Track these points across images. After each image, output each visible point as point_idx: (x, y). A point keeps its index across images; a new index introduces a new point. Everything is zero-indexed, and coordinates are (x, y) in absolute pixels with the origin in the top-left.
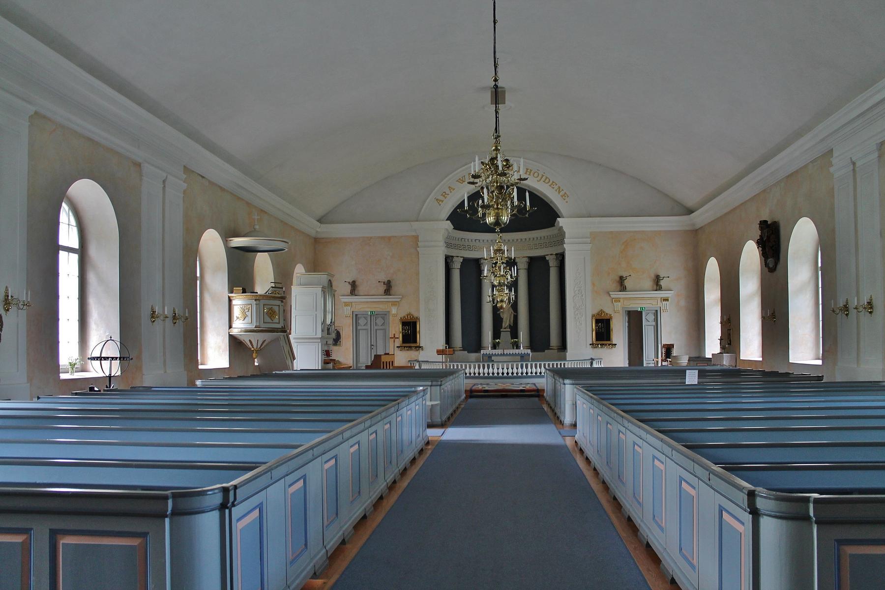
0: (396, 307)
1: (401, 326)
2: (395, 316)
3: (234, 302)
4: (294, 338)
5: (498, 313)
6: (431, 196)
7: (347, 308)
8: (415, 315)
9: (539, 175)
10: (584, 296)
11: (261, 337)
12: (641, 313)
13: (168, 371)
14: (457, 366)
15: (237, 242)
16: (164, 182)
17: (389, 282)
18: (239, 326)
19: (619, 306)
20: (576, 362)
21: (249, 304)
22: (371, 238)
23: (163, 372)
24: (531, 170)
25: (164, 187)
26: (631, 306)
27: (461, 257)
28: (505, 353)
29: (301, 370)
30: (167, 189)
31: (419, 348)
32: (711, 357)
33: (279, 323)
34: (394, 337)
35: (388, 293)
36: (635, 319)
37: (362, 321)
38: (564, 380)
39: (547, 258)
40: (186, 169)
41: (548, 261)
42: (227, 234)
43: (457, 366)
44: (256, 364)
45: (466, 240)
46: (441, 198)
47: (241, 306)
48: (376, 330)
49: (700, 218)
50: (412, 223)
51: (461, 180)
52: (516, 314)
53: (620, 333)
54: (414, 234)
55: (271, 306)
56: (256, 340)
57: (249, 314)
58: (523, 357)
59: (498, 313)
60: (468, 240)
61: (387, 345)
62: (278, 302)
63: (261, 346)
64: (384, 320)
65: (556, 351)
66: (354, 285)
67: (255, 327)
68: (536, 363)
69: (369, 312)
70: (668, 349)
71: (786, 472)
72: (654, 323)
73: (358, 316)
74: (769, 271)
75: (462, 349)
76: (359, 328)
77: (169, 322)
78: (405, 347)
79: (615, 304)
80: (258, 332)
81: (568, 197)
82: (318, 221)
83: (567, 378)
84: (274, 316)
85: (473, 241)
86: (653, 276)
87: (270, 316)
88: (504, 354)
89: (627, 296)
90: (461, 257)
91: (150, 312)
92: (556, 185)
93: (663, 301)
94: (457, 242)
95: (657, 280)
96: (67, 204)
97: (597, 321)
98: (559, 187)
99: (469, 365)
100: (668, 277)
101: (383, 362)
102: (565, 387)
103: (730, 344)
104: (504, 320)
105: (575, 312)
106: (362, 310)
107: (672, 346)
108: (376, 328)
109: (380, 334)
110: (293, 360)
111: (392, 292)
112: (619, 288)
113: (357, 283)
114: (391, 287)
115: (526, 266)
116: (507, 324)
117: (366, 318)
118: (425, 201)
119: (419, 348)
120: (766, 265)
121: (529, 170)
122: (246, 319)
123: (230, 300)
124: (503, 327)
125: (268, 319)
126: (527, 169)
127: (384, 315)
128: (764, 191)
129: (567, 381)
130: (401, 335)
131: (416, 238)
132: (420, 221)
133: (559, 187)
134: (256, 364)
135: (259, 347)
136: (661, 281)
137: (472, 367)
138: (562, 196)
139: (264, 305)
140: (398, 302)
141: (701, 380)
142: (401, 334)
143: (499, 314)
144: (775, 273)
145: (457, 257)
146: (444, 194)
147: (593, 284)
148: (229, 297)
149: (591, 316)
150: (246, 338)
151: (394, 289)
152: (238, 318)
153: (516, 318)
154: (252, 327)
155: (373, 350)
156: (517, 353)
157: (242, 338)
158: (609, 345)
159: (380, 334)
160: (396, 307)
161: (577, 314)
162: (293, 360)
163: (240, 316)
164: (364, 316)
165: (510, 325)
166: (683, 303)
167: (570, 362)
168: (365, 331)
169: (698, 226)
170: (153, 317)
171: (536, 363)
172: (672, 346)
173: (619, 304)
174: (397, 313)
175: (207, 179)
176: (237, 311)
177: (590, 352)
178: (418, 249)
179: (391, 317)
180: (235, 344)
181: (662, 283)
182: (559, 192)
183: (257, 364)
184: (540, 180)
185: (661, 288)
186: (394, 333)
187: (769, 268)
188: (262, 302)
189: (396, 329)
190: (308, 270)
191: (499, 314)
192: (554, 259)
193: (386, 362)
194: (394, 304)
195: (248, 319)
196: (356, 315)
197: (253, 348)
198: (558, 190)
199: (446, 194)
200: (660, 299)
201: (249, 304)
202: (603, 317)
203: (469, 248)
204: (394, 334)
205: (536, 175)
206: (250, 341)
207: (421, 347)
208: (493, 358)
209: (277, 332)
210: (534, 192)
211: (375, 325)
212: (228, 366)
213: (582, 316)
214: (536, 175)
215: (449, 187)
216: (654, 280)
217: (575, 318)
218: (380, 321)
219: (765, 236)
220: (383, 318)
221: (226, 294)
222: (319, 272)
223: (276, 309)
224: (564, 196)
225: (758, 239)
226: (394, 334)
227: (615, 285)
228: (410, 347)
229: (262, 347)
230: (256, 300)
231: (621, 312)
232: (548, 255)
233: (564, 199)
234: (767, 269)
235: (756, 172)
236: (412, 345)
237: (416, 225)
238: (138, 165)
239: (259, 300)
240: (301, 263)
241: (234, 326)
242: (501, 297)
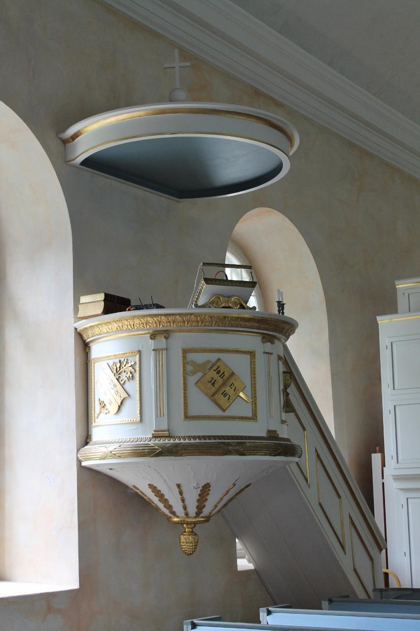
3: (96, 351)
4: (397, 478)
33: (254, 418)
44: (244, 564)
55: (213, 357)
57: (133, 387)
62: (251, 341)
67: (155, 437)
71: (50, 162)
84: (230, 391)
96: (234, 255)
110: (373, 550)
122: (125, 409)
123: (84, 346)
125: (201, 404)
134: (244, 564)
135: (192, 510)
141: (378, 451)
148: (79, 335)
162: (373, 550)
183: (251, 566)
188: (180, 340)
195: (132, 409)
206: (153, 488)
209: (242, 454)
223: (239, 365)
239: (166, 334)
241: (97, 434)
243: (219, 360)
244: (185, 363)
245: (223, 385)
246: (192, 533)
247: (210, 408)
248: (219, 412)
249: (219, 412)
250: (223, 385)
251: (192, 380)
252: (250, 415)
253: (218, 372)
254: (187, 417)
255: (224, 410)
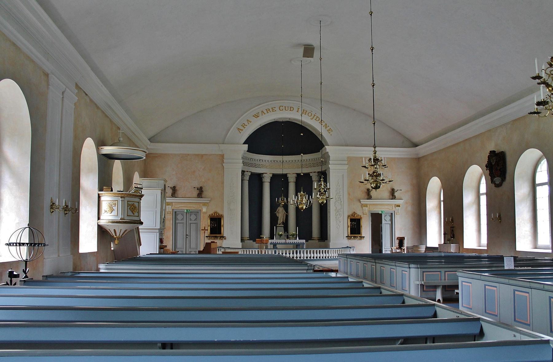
0: (206, 207)
1: (209, 221)
2: (206, 213)
3: (102, 198)
5: (275, 213)
6: (233, 126)
7: (169, 207)
8: (220, 213)
9: (312, 114)
10: (342, 202)
11: (124, 227)
12: (381, 215)
13: (60, 256)
14: (255, 252)
15: (107, 150)
16: (63, 93)
17: (201, 188)
18: (107, 217)
19: (366, 209)
20: (337, 249)
21: (116, 201)
22: (188, 155)
23: (57, 256)
24: (306, 111)
25: (63, 100)
26: (375, 210)
27: (250, 172)
28: (287, 242)
29: (151, 254)
30: (65, 99)
31: (223, 237)
32: (438, 246)
34: (205, 229)
35: (200, 197)
36: (377, 219)
37: (179, 217)
38: (409, 265)
39: (311, 175)
40: (77, 86)
41: (311, 176)
42: (100, 143)
43: (255, 252)
44: (112, 249)
45: (254, 160)
46: (242, 128)
47: (109, 202)
48: (190, 224)
49: (422, 150)
50: (220, 145)
51: (256, 116)
52: (287, 214)
53: (366, 229)
54: (220, 153)
55: (133, 203)
56: (120, 229)
57: (115, 208)
58: (297, 246)
59: (275, 213)
60: (255, 160)
61: (198, 235)
63: (122, 235)
64: (196, 216)
65: (317, 241)
66: (174, 189)
67: (120, 219)
68: (317, 250)
69: (185, 211)
70: (401, 241)
72: (390, 222)
73: (177, 213)
74: (495, 186)
75: (249, 239)
76: (177, 222)
77: (62, 213)
78: (212, 237)
79: (397, 208)
80: (123, 223)
81: (332, 131)
82: (149, 140)
83: (413, 263)
85: (259, 160)
86: (390, 189)
87: (132, 210)
88: (286, 243)
89: (372, 203)
90: (250, 172)
91: (49, 204)
92: (324, 122)
93: (397, 207)
94: (254, 161)
95: (393, 192)
97: (352, 220)
98: (326, 124)
99: (282, 250)
100: (401, 190)
101: (212, 248)
102: (410, 270)
103: (453, 237)
104: (279, 219)
105: (336, 213)
106: (180, 208)
107: (403, 238)
108: (190, 222)
109: (193, 227)
110: (139, 246)
111: (203, 196)
112: (366, 197)
113: (177, 188)
114: (203, 192)
115: (295, 180)
116: (282, 221)
117: (182, 215)
118: (229, 130)
119: (223, 237)
120: (492, 181)
121: (305, 111)
122: (112, 213)
123: (99, 197)
124: (278, 224)
126: (266, 110)
127: (197, 213)
128: (490, 131)
129: (412, 266)
130: (209, 228)
131: (222, 156)
132: (225, 144)
133: (326, 124)
135: (121, 235)
136: (395, 193)
137: (291, 253)
138: (328, 131)
139: (127, 201)
140: (207, 203)
142: (209, 227)
143: (276, 213)
144: (500, 188)
145: (247, 171)
146: (244, 125)
147: (349, 194)
148: (99, 194)
149: (347, 217)
150: (111, 228)
151: (205, 194)
152: (106, 211)
153: (287, 217)
154: (118, 219)
155: (187, 239)
156: (279, 243)
157: (107, 228)
158: (221, 237)
159: (193, 227)
160: (206, 207)
161: (337, 215)
163: (107, 210)
164: (181, 213)
165: (283, 222)
166: (410, 208)
167: (332, 250)
168: (182, 224)
169: (420, 156)
170: (52, 208)
171: (317, 250)
172: (403, 238)
173: (367, 208)
174: (206, 211)
175: (89, 97)
176: (105, 206)
177: (346, 242)
178: (223, 164)
179: (202, 215)
180: (102, 231)
181: (396, 194)
182: (326, 128)
184: (313, 118)
185: (395, 198)
186: (204, 226)
187: (495, 184)
189: (206, 223)
190: (141, 177)
191: (276, 213)
192: (316, 175)
193: (213, 248)
194: (204, 204)
195: (115, 213)
196: (175, 212)
197: (116, 236)
198: (325, 126)
199: (245, 125)
200: (394, 205)
201: (116, 201)
202: (356, 217)
203: (255, 166)
204: (205, 227)
205: (310, 114)
207: (224, 237)
208: (278, 246)
210: (307, 127)
211: (189, 220)
212: (96, 250)
213: (341, 216)
214: (310, 114)
215: (248, 120)
216: (391, 192)
217: (336, 218)
218: (193, 217)
219: (493, 161)
220: (196, 215)
221: (96, 192)
222: (147, 178)
224: (330, 131)
225: (487, 164)
226: (205, 227)
227: (364, 195)
228: (216, 237)
229: (123, 235)
230: (121, 197)
231: (368, 214)
232: (312, 172)
233: (329, 133)
234: (493, 185)
235: (484, 118)
236: (218, 235)
237: (223, 147)
238: (47, 75)
240: (137, 172)
241: (102, 217)
242: (322, 200)
243: (134, 204)
244: (127, 204)
245: (134, 209)
246: (118, 240)
247: (132, 214)
248: (133, 215)
249: (133, 215)
250: (134, 209)
251: (129, 208)
252: (137, 215)
253: (134, 206)
254: (127, 216)
255: (134, 214)
